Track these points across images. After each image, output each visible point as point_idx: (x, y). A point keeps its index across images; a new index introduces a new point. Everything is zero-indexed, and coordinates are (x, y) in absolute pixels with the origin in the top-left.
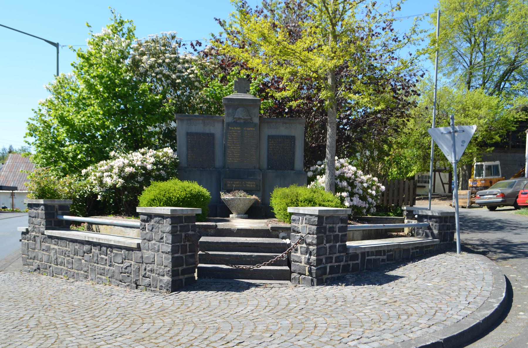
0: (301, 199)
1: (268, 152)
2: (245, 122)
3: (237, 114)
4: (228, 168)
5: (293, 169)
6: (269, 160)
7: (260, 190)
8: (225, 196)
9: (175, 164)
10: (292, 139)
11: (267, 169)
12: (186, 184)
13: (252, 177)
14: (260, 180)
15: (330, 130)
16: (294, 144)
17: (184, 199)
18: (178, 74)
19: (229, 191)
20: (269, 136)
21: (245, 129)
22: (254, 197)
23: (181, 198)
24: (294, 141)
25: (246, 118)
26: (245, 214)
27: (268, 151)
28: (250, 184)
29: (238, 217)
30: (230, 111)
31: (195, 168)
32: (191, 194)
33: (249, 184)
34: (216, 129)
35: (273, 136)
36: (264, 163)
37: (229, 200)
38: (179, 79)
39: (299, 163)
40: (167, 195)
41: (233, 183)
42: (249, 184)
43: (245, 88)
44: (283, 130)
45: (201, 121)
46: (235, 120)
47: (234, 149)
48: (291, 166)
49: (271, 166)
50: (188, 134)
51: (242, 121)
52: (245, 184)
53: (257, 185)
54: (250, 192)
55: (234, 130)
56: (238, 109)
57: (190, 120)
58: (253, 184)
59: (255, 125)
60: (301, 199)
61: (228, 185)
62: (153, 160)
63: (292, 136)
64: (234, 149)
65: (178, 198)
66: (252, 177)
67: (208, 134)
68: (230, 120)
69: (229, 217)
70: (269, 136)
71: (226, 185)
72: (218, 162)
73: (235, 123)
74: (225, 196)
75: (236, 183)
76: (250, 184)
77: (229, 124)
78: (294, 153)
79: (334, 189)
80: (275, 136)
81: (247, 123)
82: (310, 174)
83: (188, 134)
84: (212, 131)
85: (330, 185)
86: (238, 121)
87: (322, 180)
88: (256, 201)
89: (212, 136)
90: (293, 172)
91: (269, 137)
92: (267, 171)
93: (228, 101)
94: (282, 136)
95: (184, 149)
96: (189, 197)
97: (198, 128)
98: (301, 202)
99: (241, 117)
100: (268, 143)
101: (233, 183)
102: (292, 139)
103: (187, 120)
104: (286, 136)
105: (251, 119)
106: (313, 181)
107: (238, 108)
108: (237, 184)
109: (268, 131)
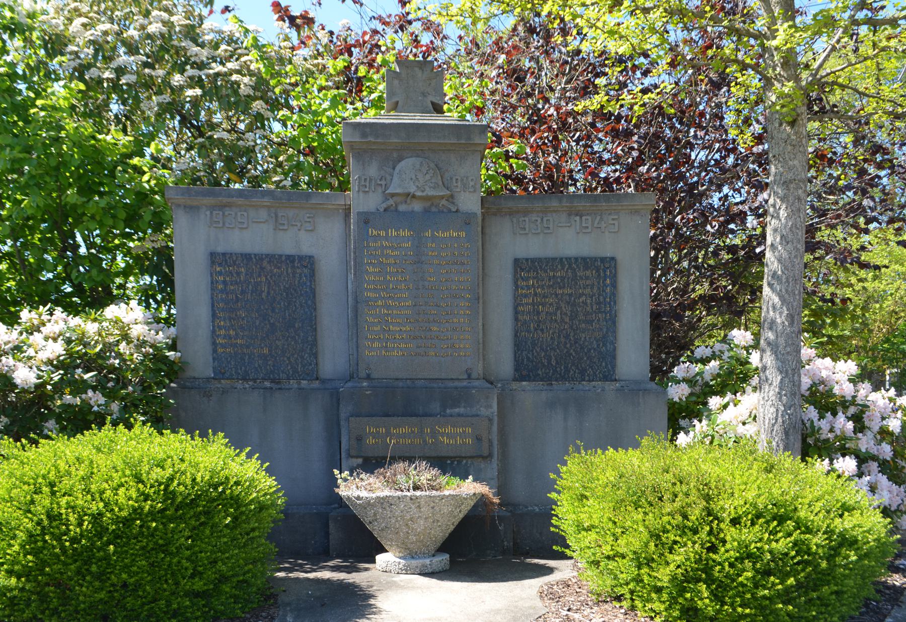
0: (728, 506)
1: (516, 319)
2: (426, 211)
3: (396, 179)
4: (368, 377)
5: (609, 376)
6: (518, 344)
7: (490, 456)
8: (357, 488)
9: (160, 366)
10: (604, 268)
11: (515, 379)
12: (174, 444)
13: (461, 410)
14: (490, 420)
15: (783, 213)
16: (614, 285)
17: (127, 522)
18: (190, 71)
19: (372, 464)
20: (516, 261)
21: (428, 234)
22: (470, 488)
23: (117, 520)
24: (614, 277)
25: (431, 193)
26: (442, 549)
27: (516, 312)
28: (453, 436)
29: (408, 571)
30: (373, 171)
31: (245, 379)
32: (169, 495)
33: (449, 436)
34: (322, 241)
35: (533, 260)
36: (503, 361)
37: (368, 504)
38: (192, 87)
39: (632, 352)
40: (44, 501)
41: (388, 433)
42: (449, 436)
43: (424, 94)
44: (568, 240)
45: (263, 214)
46: (391, 202)
47: (388, 307)
48: (602, 365)
49: (525, 370)
50: (214, 258)
51: (417, 206)
52: (434, 434)
53: (479, 439)
54: (450, 464)
55: (386, 238)
56: (403, 163)
57: (222, 207)
58: (463, 435)
59: (467, 220)
60: (728, 506)
61: (370, 441)
62: (57, 349)
63: (603, 260)
64: (388, 307)
65: (97, 518)
66: (461, 410)
67: (290, 259)
68: (372, 202)
69: (374, 562)
70: (516, 261)
71: (359, 439)
72: (332, 358)
73: (391, 214)
74: (357, 488)
75: (401, 432)
76: (453, 436)
77: (366, 219)
78: (613, 321)
79: (798, 445)
80: (540, 260)
81: (439, 211)
82: (678, 392)
83: (214, 258)
84: (306, 249)
85: (786, 433)
86: (402, 208)
87: (748, 414)
88: (482, 502)
89: (308, 263)
90: (610, 386)
91: (518, 264)
92: (515, 385)
93: (364, 135)
94: (569, 259)
95: (203, 312)
96: (153, 514)
97: (254, 236)
98: (735, 522)
99: (412, 189)
100: (517, 287)
101: (388, 433)
102: (604, 268)
103: (212, 208)
104: (584, 259)
105: (451, 198)
106: (699, 416)
107: (400, 159)
108: (404, 436)
109: (516, 242)
